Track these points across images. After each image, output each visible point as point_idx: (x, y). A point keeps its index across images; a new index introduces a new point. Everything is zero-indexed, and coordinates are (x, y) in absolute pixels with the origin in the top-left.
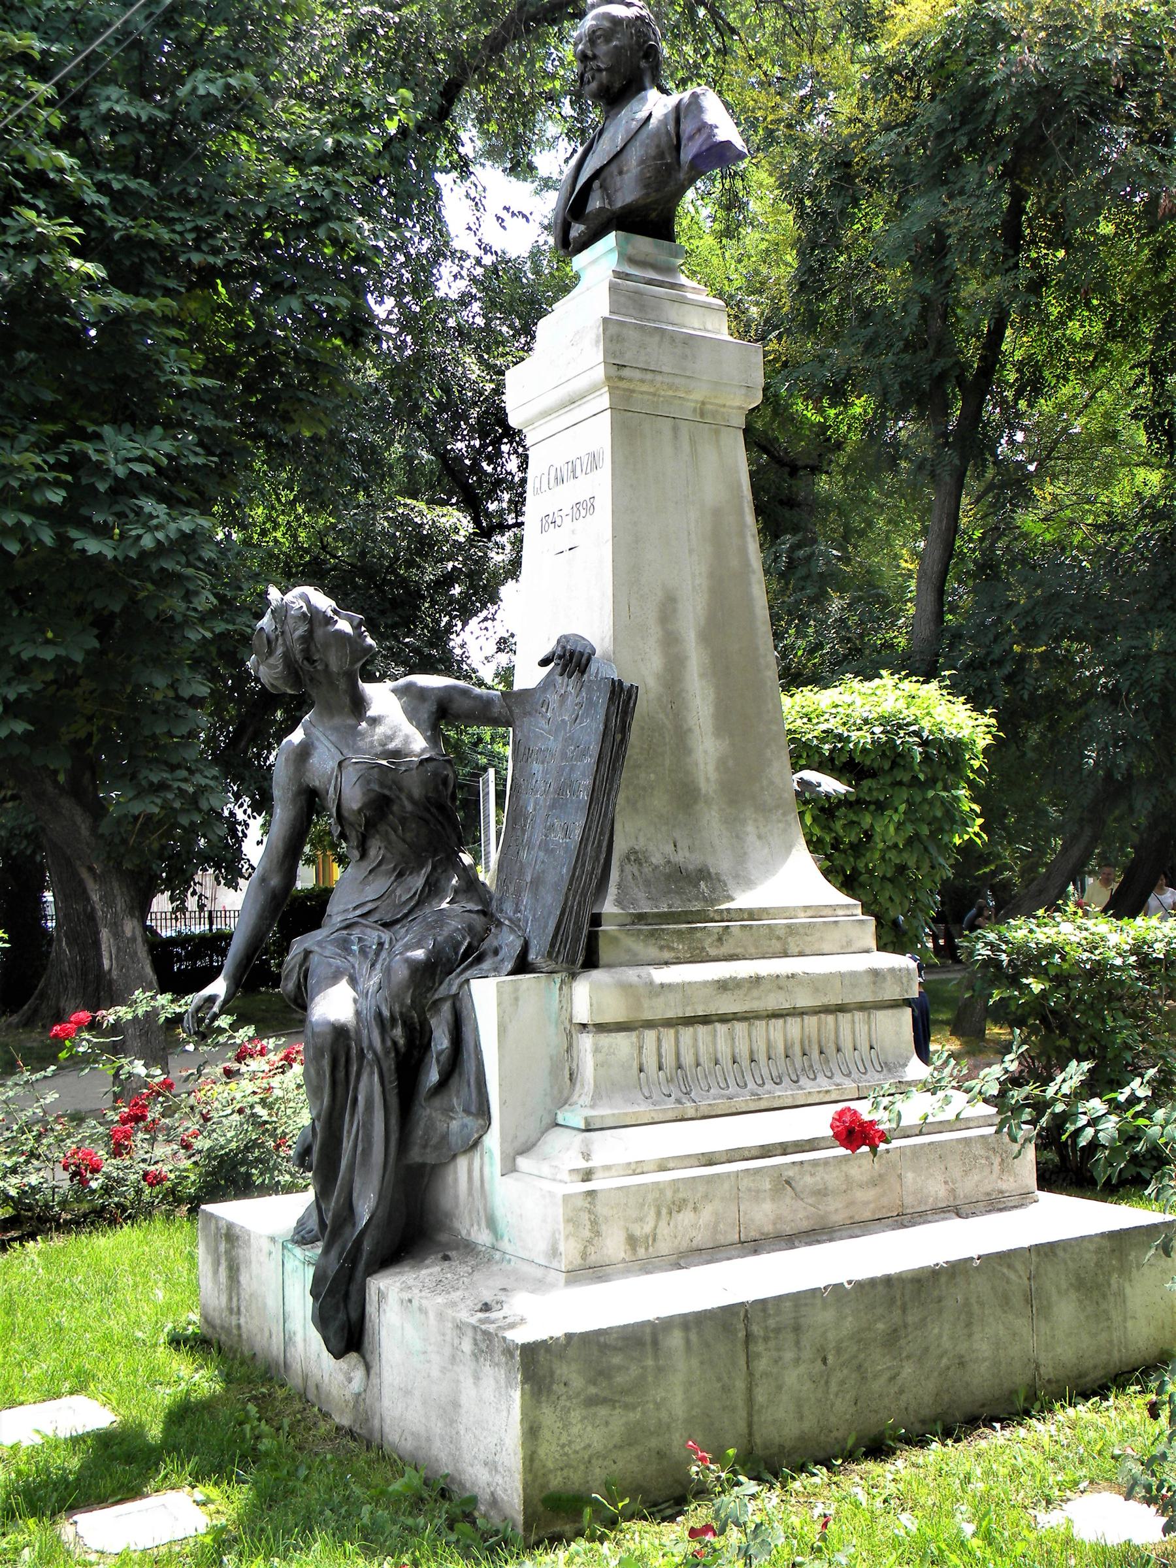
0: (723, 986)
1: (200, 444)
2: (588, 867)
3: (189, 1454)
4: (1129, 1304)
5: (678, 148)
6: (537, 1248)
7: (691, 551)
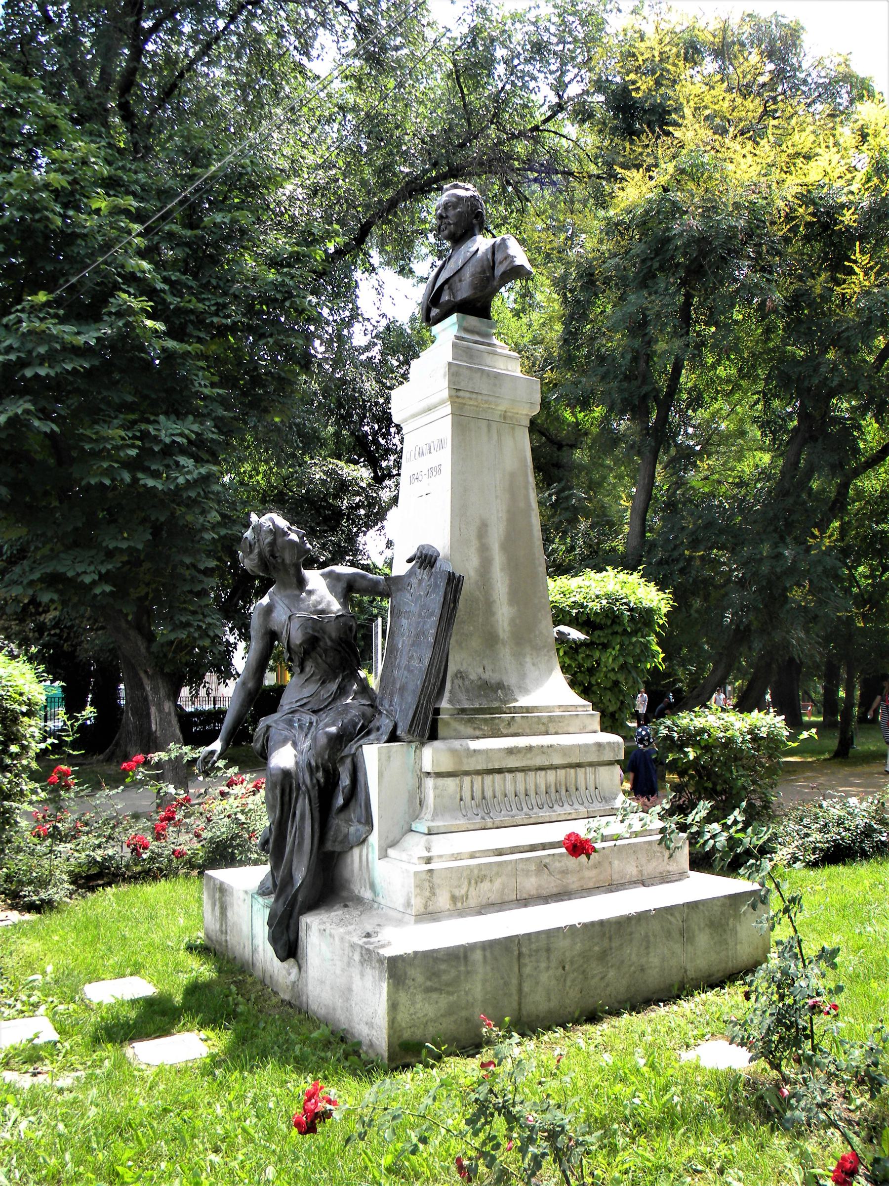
0: (510, 751)
1: (215, 426)
2: (432, 681)
3: (197, 1012)
4: (739, 935)
5: (493, 268)
6: (399, 901)
7: (497, 497)
